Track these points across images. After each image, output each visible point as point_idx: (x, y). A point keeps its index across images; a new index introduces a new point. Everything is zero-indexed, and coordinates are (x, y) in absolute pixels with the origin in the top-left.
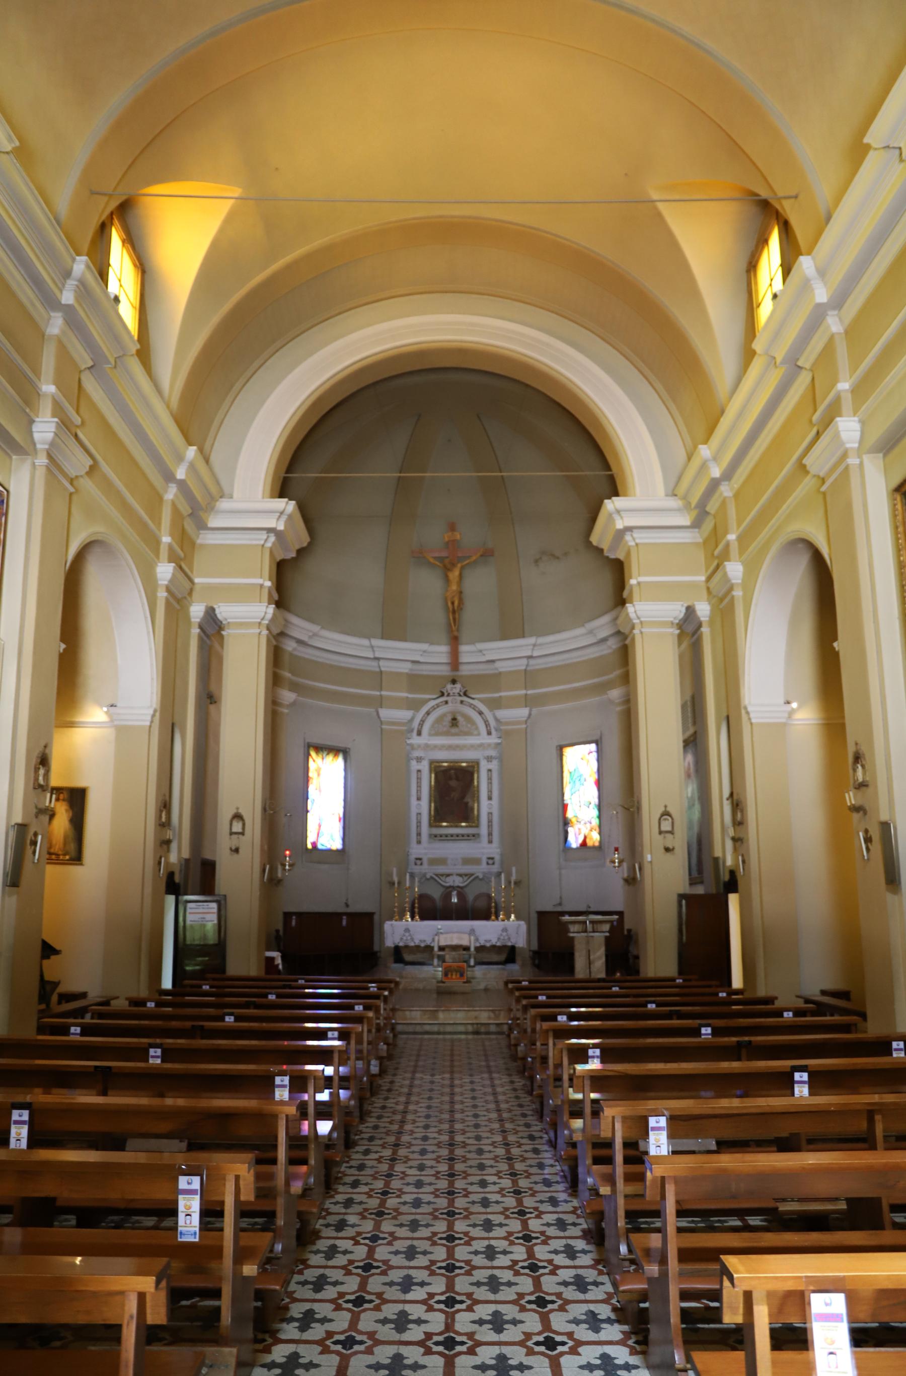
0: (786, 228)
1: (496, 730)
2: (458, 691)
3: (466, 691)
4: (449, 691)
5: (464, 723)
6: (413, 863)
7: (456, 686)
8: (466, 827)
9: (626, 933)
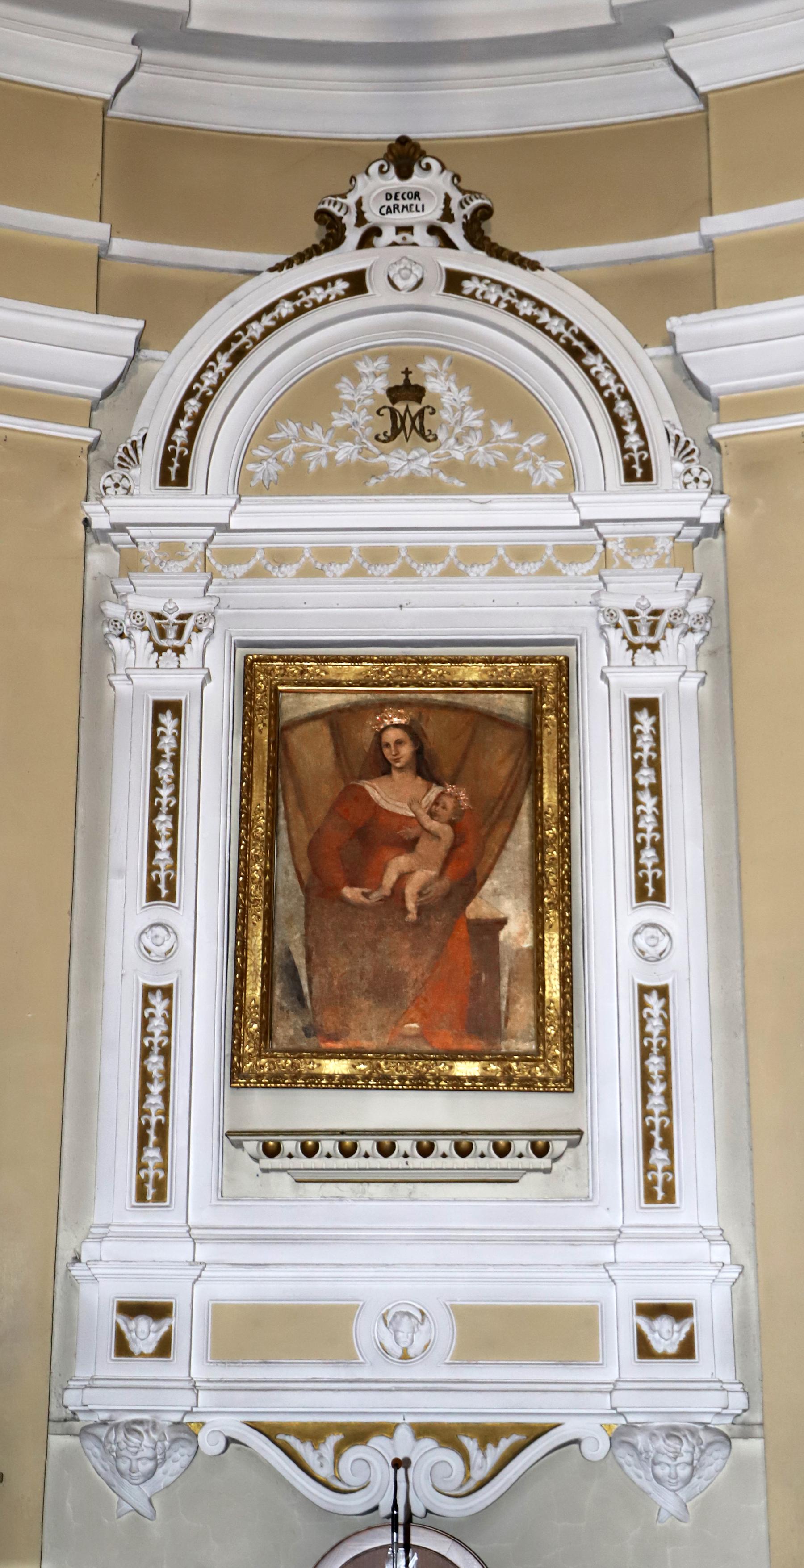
0: (711, 620)
1: (684, 450)
2: (433, 212)
3: (485, 212)
4: (373, 216)
5: (472, 418)
6: (109, 1342)
7: (417, 180)
8: (488, 1083)
9: (156, 804)
